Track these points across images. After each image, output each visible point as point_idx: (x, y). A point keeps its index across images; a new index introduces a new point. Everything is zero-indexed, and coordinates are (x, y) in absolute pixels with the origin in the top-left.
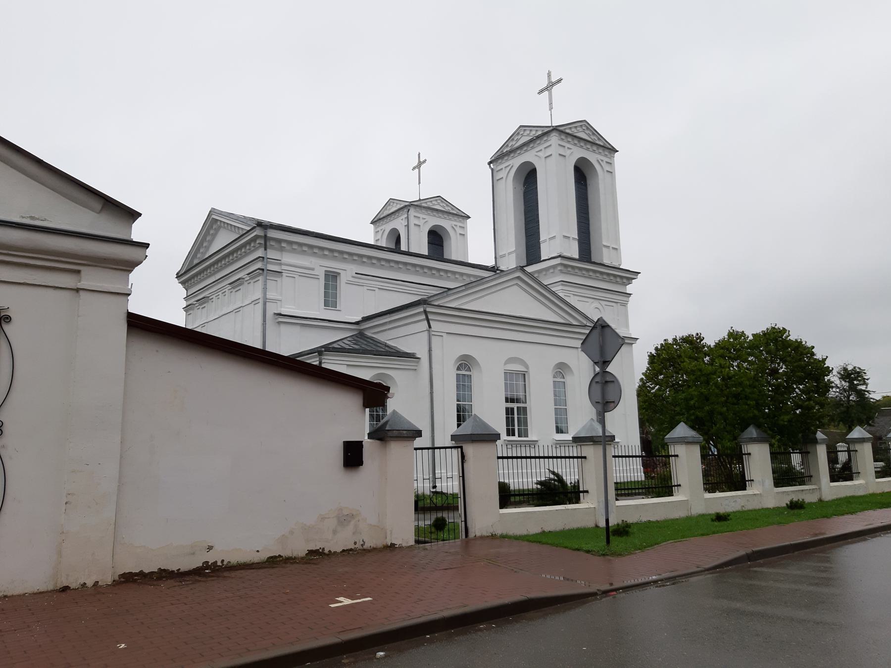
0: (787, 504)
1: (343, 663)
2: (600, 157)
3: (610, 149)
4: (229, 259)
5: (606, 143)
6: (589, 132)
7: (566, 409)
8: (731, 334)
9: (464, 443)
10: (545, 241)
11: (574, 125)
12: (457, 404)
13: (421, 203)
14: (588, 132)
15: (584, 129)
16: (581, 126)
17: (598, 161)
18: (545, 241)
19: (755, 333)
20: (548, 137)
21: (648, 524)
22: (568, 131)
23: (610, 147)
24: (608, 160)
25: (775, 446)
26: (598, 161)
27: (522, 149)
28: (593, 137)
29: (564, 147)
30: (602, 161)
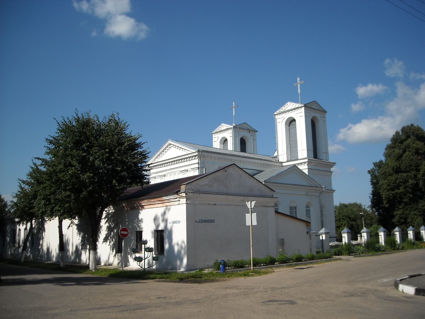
1: (145, 182)
3: (324, 112)
4: (68, 163)
5: (322, 109)
7: (309, 210)
8: (384, 156)
9: (140, 270)
10: (300, 151)
11: (311, 103)
12: (306, 209)
14: (316, 105)
16: (313, 103)
18: (300, 151)
19: (374, 162)
20: (301, 108)
21: (415, 227)
22: (309, 106)
23: (324, 111)
25: (335, 210)
27: (292, 111)
28: (318, 107)
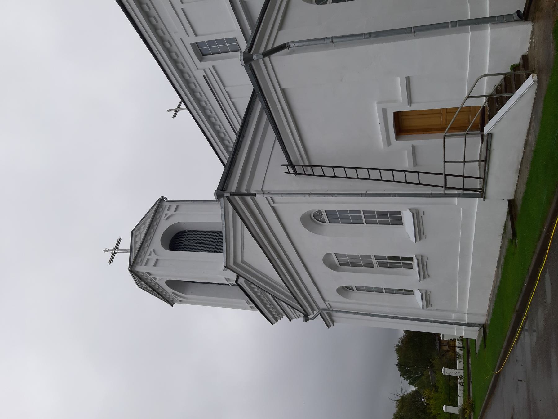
0: (518, 12)
2: (163, 218)
6: (142, 227)
13: (135, 249)
15: (139, 233)
17: (167, 219)
23: (158, 203)
24: (174, 206)
26: (167, 219)
29: (148, 259)
30: (166, 214)
